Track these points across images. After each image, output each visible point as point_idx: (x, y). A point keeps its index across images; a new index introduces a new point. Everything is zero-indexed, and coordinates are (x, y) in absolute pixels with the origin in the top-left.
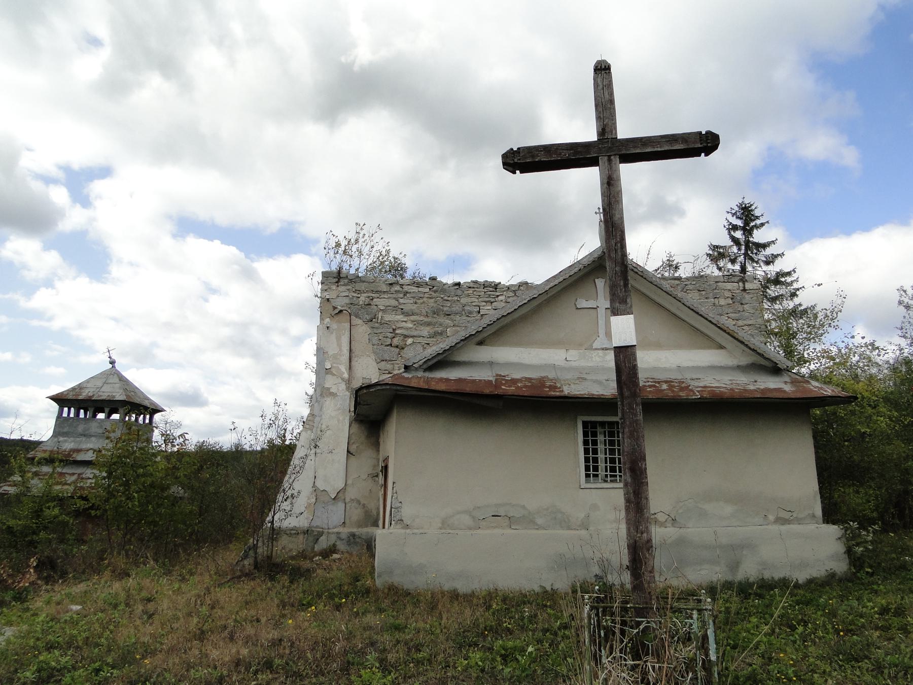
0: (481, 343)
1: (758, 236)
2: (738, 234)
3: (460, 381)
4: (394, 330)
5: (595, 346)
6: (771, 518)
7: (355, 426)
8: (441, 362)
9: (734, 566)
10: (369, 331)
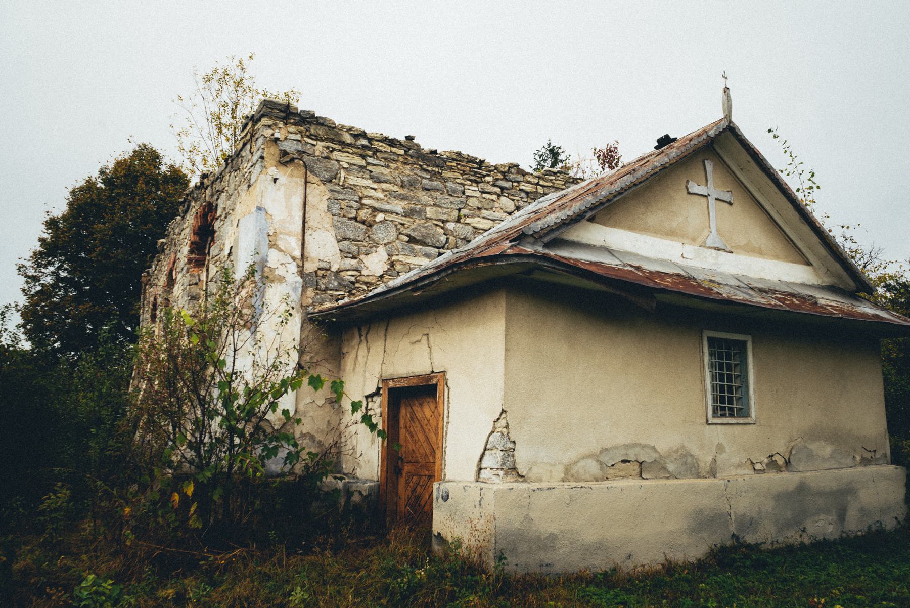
3: (577, 260)
10: (328, 195)
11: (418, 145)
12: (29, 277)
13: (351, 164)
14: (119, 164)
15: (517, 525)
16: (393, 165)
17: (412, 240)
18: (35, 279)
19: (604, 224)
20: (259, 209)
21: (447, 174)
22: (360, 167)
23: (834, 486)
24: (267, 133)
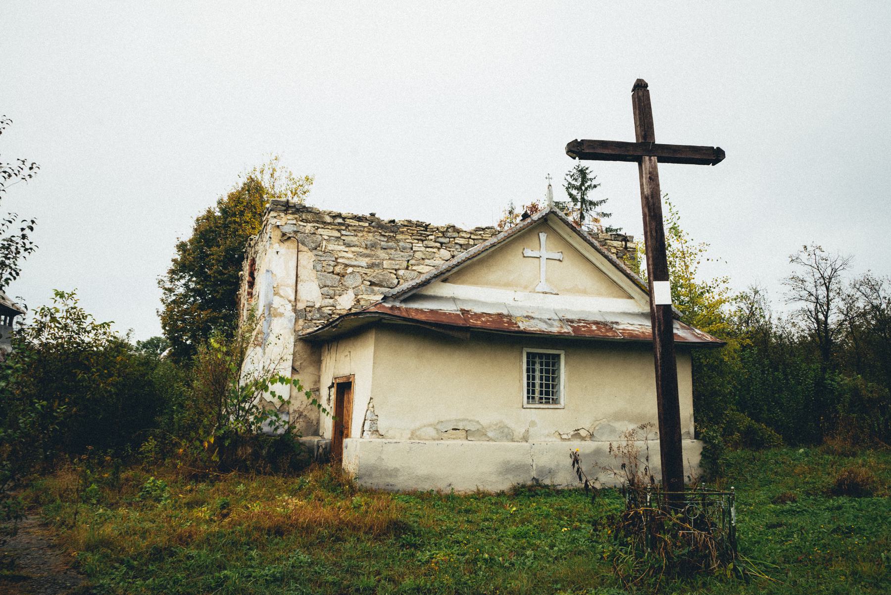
0: (445, 281)
1: (591, 195)
4: (336, 259)
5: (538, 289)
7: (300, 345)
8: (415, 294)
10: (314, 258)
11: (378, 219)
12: (166, 289)
14: (231, 197)
15: (373, 462)
16: (360, 234)
17: (372, 284)
18: (170, 290)
19: (454, 283)
20: (268, 271)
21: (399, 237)
24: (273, 221)
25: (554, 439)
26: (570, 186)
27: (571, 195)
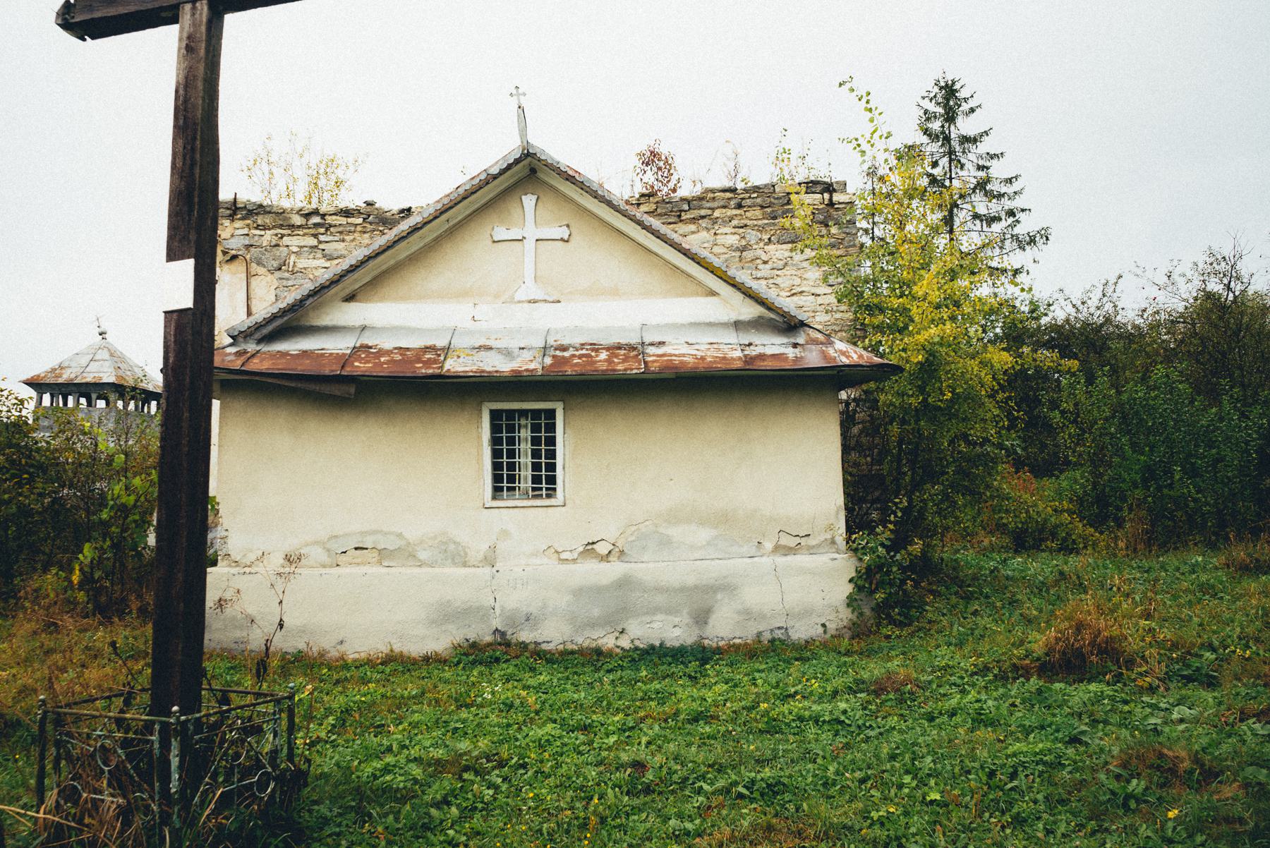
0: (350, 298)
1: (965, 126)
2: (936, 126)
3: (305, 353)
5: (518, 297)
6: (769, 546)
8: (289, 322)
9: (702, 617)
13: (301, 247)
16: (348, 238)
19: (367, 301)
22: (312, 247)
23: (691, 581)
25: (546, 560)
26: (929, 116)
27: (926, 132)
